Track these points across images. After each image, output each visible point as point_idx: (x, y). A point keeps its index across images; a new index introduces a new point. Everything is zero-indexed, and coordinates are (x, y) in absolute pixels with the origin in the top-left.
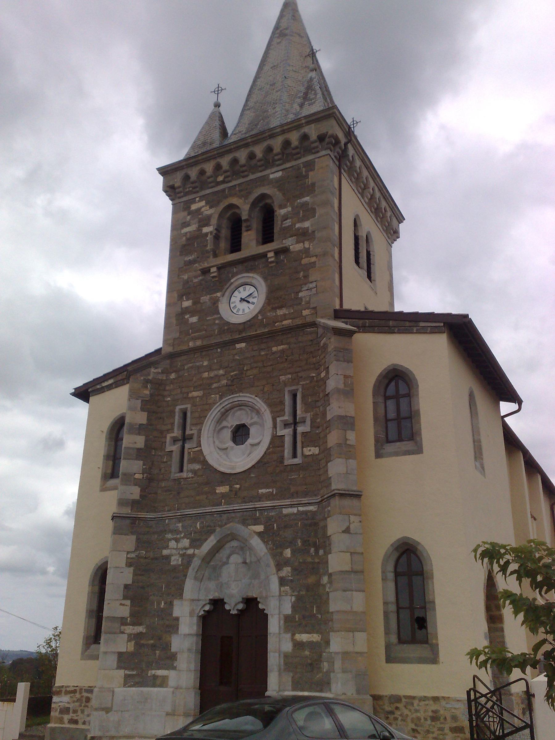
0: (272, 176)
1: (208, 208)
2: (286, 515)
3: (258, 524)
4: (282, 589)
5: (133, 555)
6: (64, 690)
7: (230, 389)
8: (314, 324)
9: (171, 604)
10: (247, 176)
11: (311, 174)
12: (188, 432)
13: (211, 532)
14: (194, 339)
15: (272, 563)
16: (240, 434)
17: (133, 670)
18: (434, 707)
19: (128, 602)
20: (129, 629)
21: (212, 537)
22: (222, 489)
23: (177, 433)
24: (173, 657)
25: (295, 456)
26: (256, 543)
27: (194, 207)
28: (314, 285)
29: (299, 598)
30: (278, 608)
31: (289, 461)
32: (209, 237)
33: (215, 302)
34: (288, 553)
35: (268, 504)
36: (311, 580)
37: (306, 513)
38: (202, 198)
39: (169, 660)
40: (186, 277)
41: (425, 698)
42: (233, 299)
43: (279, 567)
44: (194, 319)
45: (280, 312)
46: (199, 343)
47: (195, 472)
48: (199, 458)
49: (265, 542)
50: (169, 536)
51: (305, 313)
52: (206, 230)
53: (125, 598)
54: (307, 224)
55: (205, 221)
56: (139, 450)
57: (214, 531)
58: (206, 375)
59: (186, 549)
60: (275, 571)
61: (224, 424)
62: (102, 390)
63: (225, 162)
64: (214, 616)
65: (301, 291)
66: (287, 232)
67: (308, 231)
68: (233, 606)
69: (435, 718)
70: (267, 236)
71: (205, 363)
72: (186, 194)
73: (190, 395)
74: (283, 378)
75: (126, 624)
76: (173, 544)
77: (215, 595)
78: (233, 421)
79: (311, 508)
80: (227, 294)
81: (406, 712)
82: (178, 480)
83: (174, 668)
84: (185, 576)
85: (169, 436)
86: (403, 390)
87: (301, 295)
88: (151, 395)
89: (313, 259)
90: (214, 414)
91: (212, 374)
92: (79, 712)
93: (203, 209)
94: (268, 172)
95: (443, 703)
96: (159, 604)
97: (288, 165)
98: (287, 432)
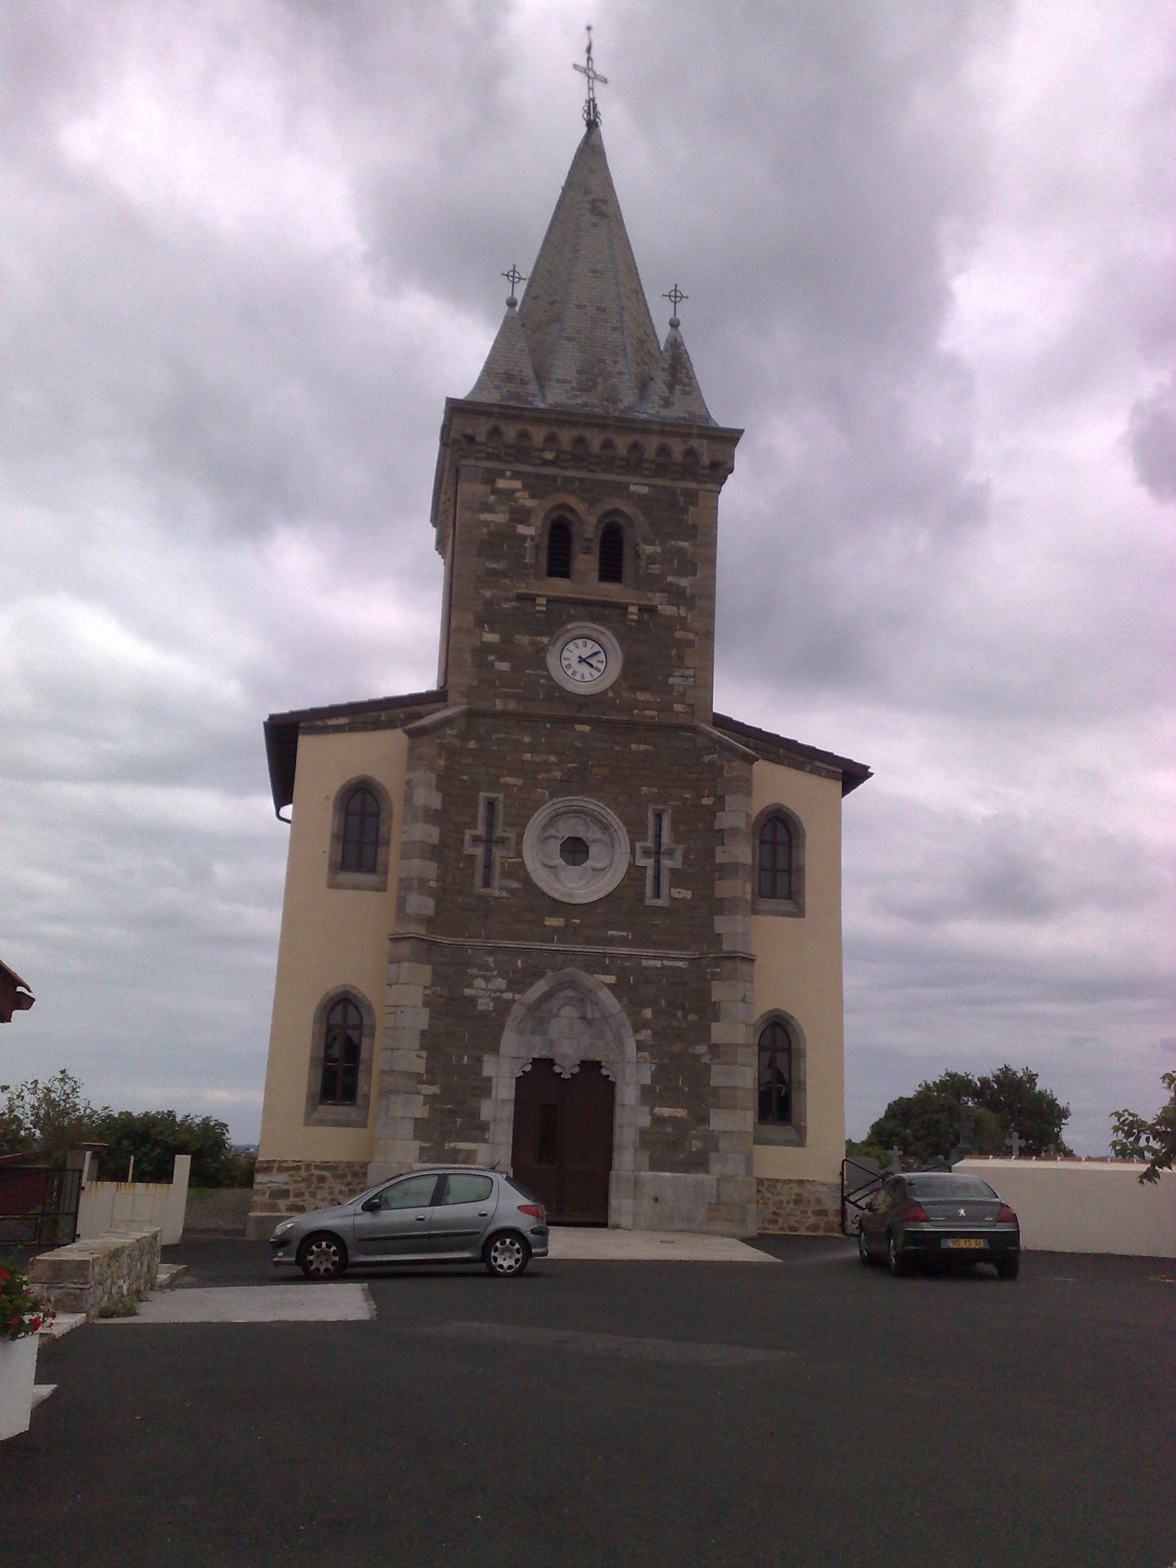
0: (632, 488)
1: (526, 494)
2: (646, 968)
3: (608, 974)
4: (640, 1054)
5: (428, 992)
6: (276, 1165)
7: (566, 786)
8: (694, 729)
9: (479, 1060)
10: (594, 471)
11: (692, 509)
12: (499, 833)
13: (540, 975)
14: (507, 696)
15: (628, 1024)
16: (575, 850)
17: (427, 1141)
18: (797, 1191)
19: (424, 1054)
20: (428, 1090)
21: (542, 982)
22: (550, 922)
23: (481, 831)
24: (484, 1127)
25: (657, 895)
26: (606, 996)
27: (502, 484)
28: (691, 672)
29: (661, 1067)
30: (632, 1077)
31: (650, 901)
32: (528, 544)
33: (542, 650)
34: (648, 1013)
35: (624, 951)
36: (677, 1047)
37: (672, 968)
38: (516, 475)
39: (478, 1130)
40: (488, 594)
41: (790, 1181)
42: (566, 654)
43: (636, 1029)
44: (503, 666)
45: (642, 697)
46: (512, 706)
47: (511, 891)
48: (518, 871)
49: (619, 998)
50: (475, 971)
51: (678, 707)
52: (522, 529)
53: (422, 1048)
54: (684, 582)
55: (521, 515)
56: (433, 846)
57: (545, 974)
58: (528, 757)
59: (502, 992)
60: (631, 1031)
61: (551, 831)
62: (325, 730)
63: (566, 436)
64: (538, 1077)
65: (672, 675)
66: (656, 583)
67: (685, 592)
68: (566, 1067)
69: (798, 1201)
70: (611, 570)
71: (527, 740)
72: (489, 457)
73: (502, 780)
74: (644, 789)
75: (421, 1082)
76: (479, 983)
77: (544, 1054)
78: (569, 828)
79: (680, 964)
80: (560, 644)
81: (768, 1195)
82: (484, 899)
83: (485, 1141)
84: (502, 1027)
85: (468, 834)
86: (782, 836)
87: (671, 680)
88: (446, 767)
89: (691, 636)
90: (540, 816)
91: (538, 759)
92: (307, 1196)
93: (518, 494)
94: (627, 479)
95: (808, 1186)
96: (460, 1058)
97: (659, 482)
98: (649, 862)
